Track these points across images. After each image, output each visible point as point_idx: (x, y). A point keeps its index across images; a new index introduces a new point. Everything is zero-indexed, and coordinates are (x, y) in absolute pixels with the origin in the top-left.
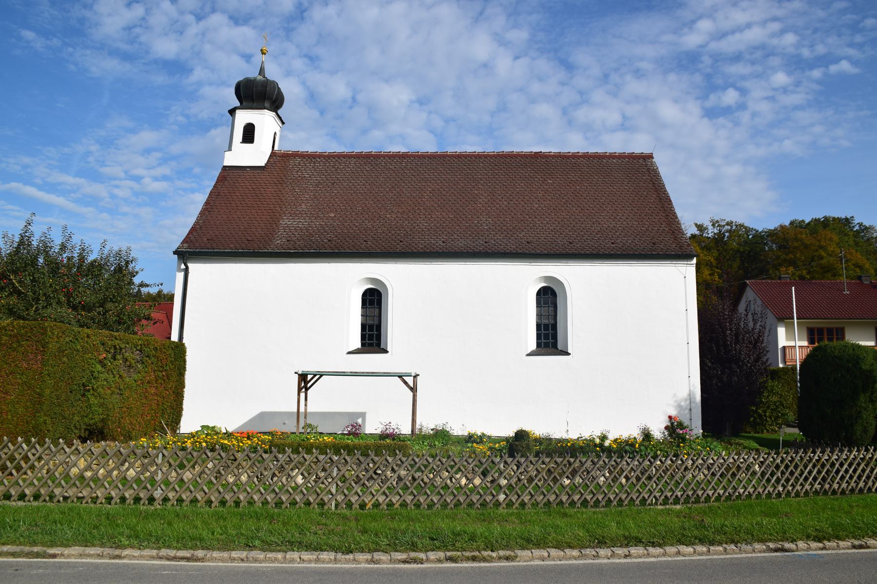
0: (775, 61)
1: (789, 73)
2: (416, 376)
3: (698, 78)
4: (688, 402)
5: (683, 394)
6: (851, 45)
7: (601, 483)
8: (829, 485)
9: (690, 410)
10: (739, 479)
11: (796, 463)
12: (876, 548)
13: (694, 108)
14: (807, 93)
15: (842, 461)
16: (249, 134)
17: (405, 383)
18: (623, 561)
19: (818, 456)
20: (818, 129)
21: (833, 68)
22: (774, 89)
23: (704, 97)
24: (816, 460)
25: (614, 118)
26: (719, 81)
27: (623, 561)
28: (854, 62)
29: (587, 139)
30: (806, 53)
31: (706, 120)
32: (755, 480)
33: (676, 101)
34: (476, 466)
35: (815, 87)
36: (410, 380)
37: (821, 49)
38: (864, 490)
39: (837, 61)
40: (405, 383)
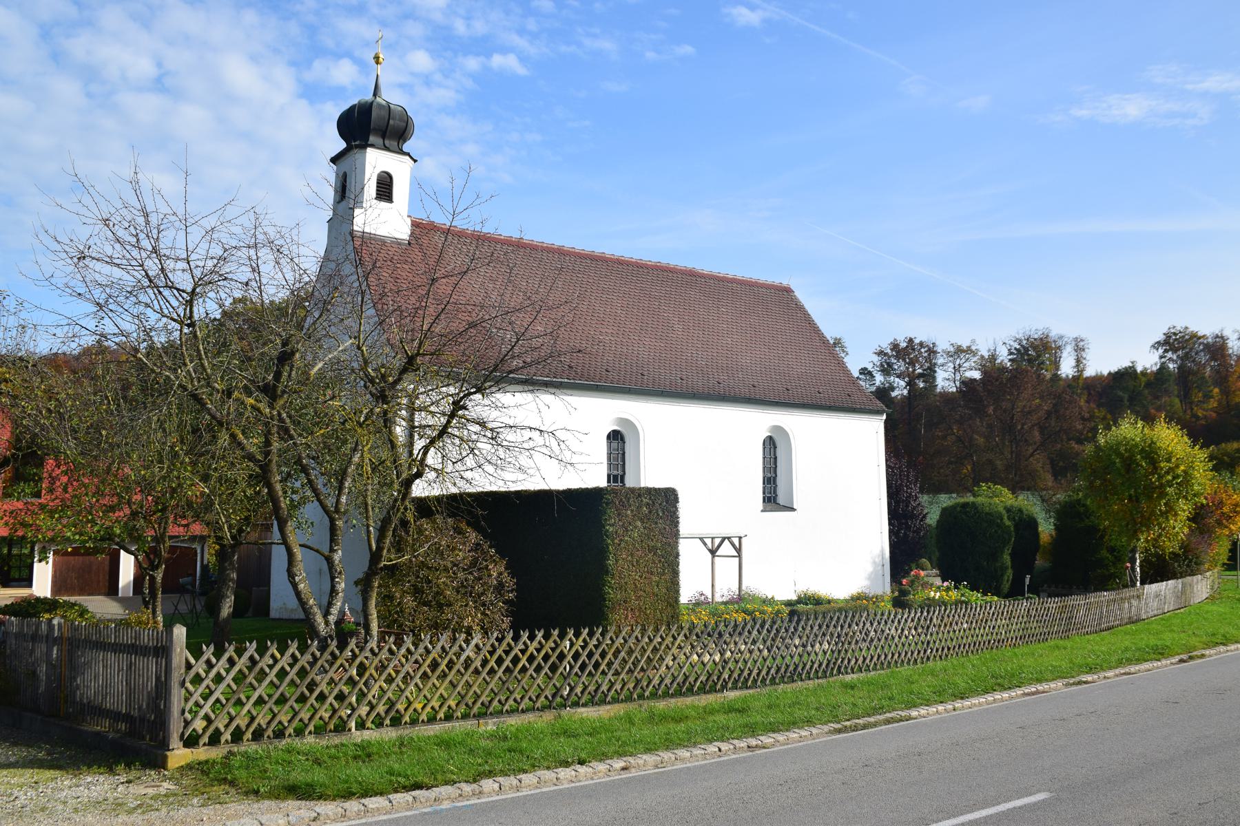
0: (415, 29)
1: (433, 53)
2: (740, 538)
3: (293, 29)
4: (880, 558)
5: (877, 551)
6: (521, 32)
7: (706, 661)
8: (368, 708)
9: (883, 565)
10: (561, 673)
11: (532, 654)
12: (1237, 642)
13: (284, 76)
14: (457, 91)
15: (577, 650)
16: (385, 189)
17: (705, 544)
18: (474, 801)
19: (598, 640)
20: (471, 149)
21: (497, 60)
22: (413, 74)
23: (299, 64)
24: (594, 646)
25: (144, 67)
26: (330, 43)
27: (474, 801)
28: (523, 59)
29: (89, 95)
30: (460, 27)
31: (303, 103)
32: (493, 682)
33: (254, 59)
34: (682, 641)
35: (469, 84)
36: (736, 541)
37: (480, 27)
38: (244, 733)
39: (504, 50)
40: (705, 544)
